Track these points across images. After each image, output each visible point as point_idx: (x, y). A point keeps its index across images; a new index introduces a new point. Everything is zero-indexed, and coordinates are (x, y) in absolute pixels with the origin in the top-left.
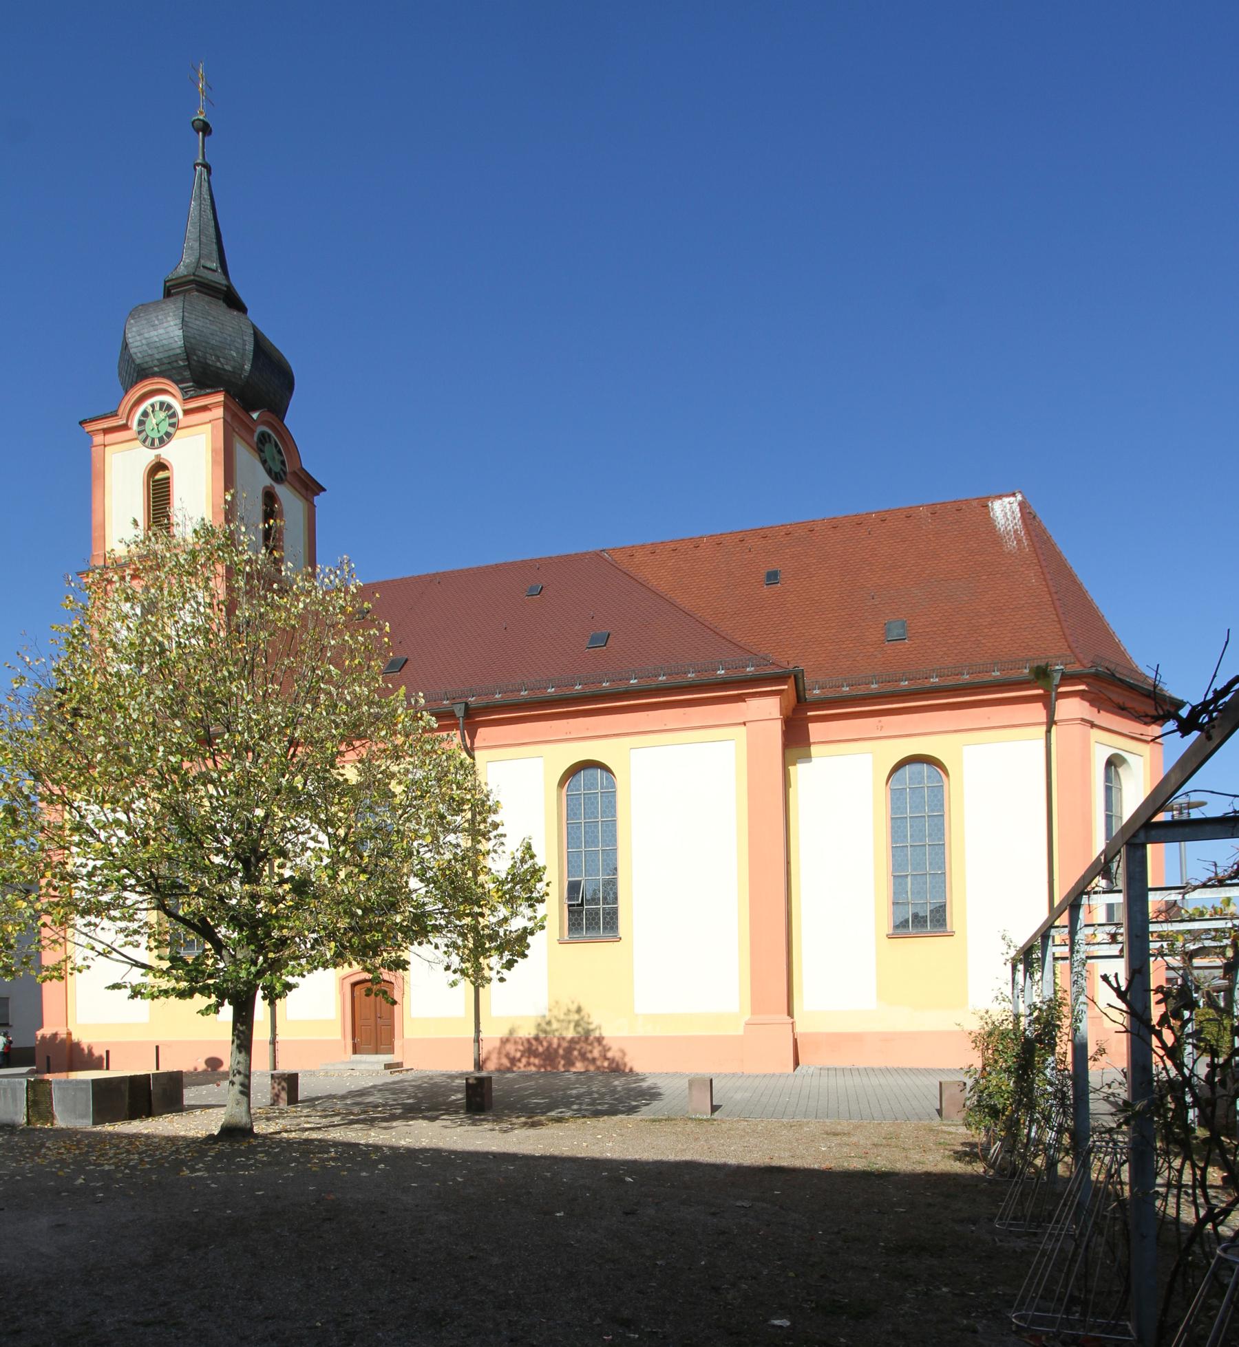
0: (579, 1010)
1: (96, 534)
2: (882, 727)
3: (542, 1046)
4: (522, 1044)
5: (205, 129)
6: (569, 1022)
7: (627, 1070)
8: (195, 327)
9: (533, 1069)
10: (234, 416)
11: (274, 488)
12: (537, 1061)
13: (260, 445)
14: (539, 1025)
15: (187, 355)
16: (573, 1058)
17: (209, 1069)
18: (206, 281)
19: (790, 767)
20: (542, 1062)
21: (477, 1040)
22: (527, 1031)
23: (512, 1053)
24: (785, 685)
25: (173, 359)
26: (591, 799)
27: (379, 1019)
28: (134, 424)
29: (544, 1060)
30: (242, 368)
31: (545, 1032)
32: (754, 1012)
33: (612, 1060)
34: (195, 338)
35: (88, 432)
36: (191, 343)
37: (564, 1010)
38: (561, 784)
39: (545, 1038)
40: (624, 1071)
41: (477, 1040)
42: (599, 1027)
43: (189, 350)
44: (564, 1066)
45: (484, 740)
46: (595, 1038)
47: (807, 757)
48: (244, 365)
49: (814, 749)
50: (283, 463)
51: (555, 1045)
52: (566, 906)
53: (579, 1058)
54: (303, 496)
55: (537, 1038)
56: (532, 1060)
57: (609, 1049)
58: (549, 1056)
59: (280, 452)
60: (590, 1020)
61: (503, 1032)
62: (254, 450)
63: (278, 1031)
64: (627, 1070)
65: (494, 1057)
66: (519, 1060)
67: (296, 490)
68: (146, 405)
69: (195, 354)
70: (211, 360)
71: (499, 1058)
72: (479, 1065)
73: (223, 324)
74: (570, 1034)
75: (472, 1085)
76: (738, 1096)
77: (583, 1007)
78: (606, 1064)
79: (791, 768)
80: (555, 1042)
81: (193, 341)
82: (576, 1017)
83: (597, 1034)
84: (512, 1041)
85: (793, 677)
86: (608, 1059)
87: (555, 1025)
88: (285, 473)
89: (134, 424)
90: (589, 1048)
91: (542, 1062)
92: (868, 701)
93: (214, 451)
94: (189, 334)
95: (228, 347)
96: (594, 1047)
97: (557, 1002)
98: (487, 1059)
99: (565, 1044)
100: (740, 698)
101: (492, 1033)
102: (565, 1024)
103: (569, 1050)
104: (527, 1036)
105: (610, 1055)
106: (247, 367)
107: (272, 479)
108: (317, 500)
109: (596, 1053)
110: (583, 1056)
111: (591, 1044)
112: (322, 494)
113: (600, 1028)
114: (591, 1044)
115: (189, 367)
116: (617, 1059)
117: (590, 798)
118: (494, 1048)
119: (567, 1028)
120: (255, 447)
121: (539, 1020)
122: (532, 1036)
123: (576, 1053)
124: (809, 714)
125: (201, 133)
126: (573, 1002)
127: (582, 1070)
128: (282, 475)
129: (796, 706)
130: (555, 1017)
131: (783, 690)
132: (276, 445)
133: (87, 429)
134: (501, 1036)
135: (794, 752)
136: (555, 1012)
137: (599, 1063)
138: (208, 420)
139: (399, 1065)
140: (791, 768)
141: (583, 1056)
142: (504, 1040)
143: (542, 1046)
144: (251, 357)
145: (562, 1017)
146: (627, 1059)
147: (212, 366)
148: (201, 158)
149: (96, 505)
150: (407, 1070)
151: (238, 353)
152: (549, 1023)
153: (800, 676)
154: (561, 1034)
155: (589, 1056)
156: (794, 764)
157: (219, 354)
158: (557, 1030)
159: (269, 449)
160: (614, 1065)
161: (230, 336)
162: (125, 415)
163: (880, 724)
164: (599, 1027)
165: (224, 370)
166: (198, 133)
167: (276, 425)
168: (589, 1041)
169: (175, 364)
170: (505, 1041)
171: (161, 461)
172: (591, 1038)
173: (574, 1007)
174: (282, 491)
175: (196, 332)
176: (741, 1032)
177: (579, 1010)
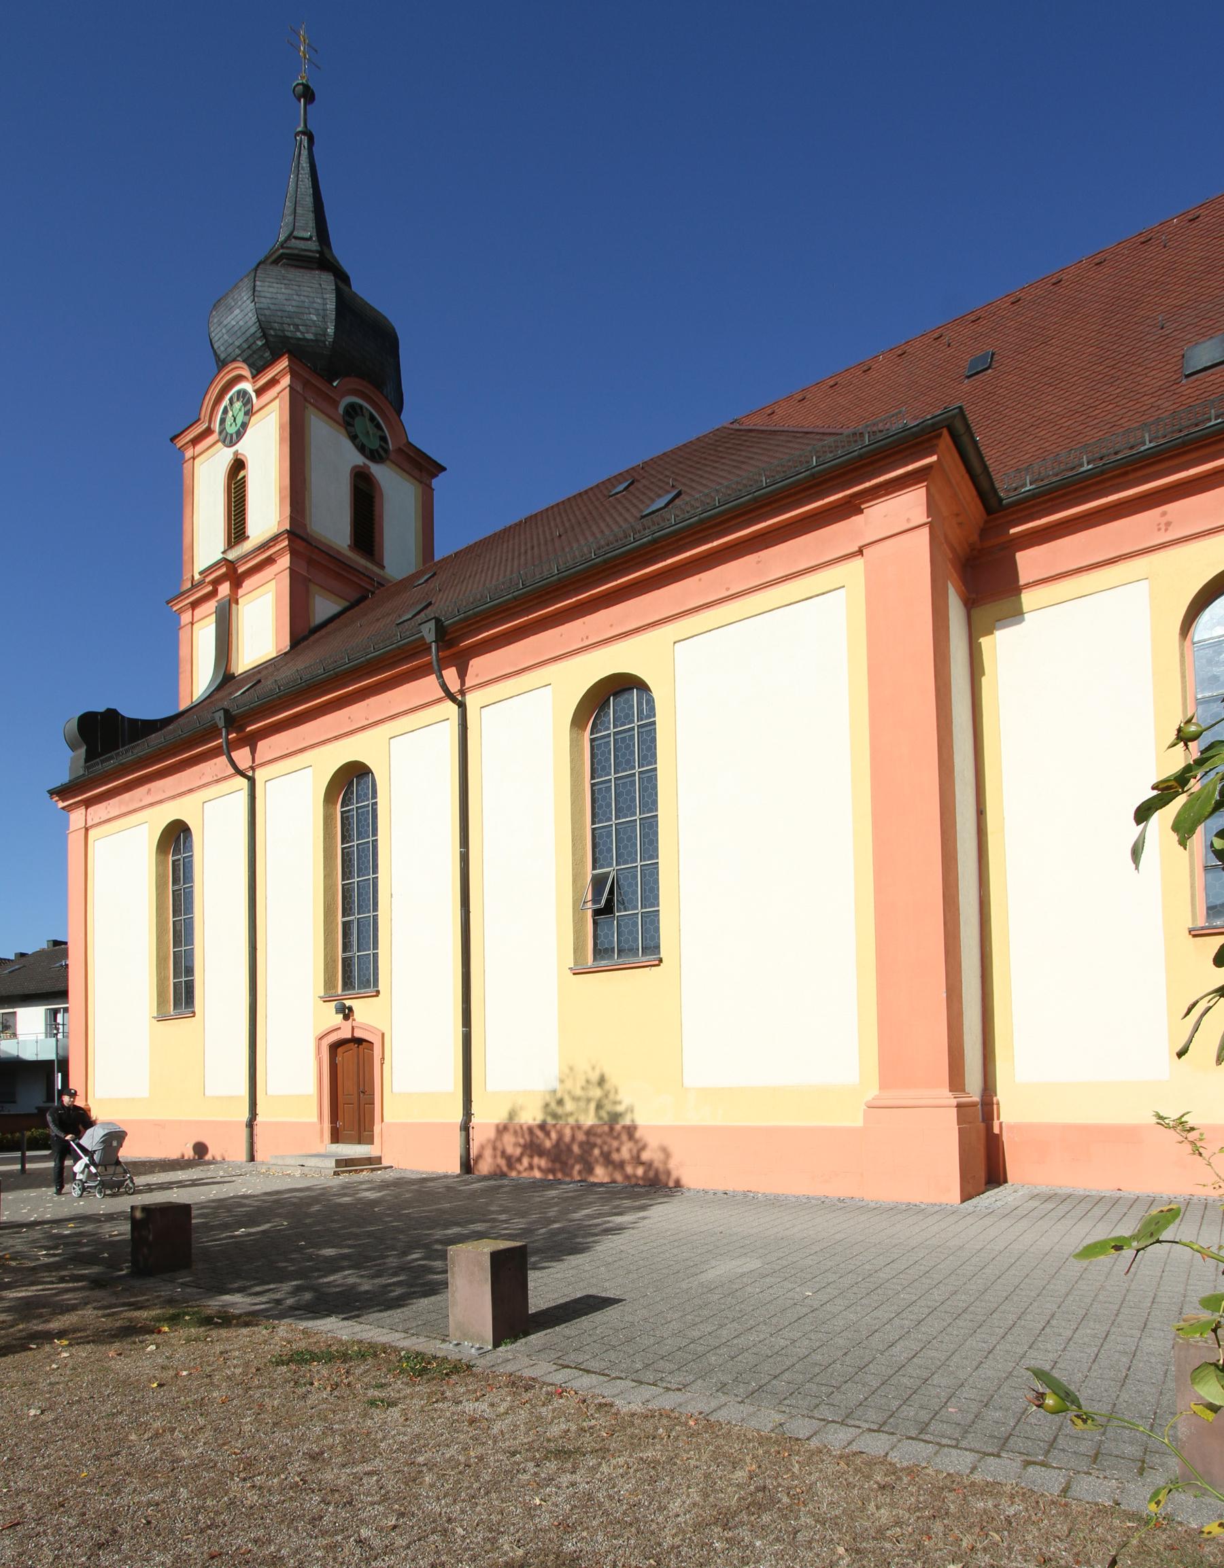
0: (602, 1081)
1: (186, 557)
2: (1168, 524)
3: (550, 1139)
4: (523, 1136)
5: (308, 94)
6: (589, 1100)
7: (671, 1184)
8: (268, 295)
9: (537, 1174)
10: (306, 384)
11: (369, 468)
12: (543, 1163)
13: (347, 418)
14: (547, 1105)
15: (263, 331)
16: (592, 1160)
17: (197, 1157)
18: (296, 252)
19: (982, 640)
20: (550, 1165)
21: (466, 1127)
22: (531, 1116)
23: (510, 1150)
24: (931, 456)
25: (251, 341)
26: (623, 742)
27: (362, 1095)
28: (216, 426)
29: (553, 1161)
30: (325, 334)
31: (555, 1116)
32: (883, 1085)
33: (648, 1165)
34: (269, 308)
35: (179, 449)
36: (265, 315)
37: (581, 1082)
38: (578, 721)
39: (554, 1126)
40: (666, 1186)
41: (466, 1127)
42: (631, 1109)
43: (264, 327)
44: (580, 1172)
45: (477, 675)
46: (624, 1127)
47: (1017, 614)
48: (326, 329)
49: (1028, 599)
50: (383, 439)
51: (567, 1138)
52: (589, 913)
53: (601, 1160)
54: (415, 478)
55: (543, 1127)
56: (536, 1160)
57: (644, 1148)
58: (560, 1156)
59: (378, 427)
60: (619, 1098)
61: (500, 1117)
62: (340, 425)
63: (475, 1108)
64: (671, 1184)
65: (488, 1153)
66: (519, 1160)
67: (407, 472)
68: (226, 402)
69: (271, 329)
70: (290, 331)
71: (495, 1157)
72: (467, 1166)
73: (299, 286)
74: (589, 1120)
75: (141, 1220)
76: (719, 1270)
77: (607, 1077)
78: (640, 1171)
79: (985, 641)
80: (568, 1133)
81: (267, 312)
82: (597, 1093)
83: (627, 1121)
84: (512, 1130)
85: (945, 431)
86: (642, 1163)
87: (569, 1106)
88: (386, 451)
89: (216, 426)
90: (615, 1144)
91: (550, 1165)
92: (1131, 476)
93: (281, 427)
94: (262, 306)
95: (307, 311)
96: (622, 1143)
97: (571, 1069)
98: (479, 1157)
99: (581, 1137)
100: (851, 508)
101: (487, 1116)
102: (582, 1104)
103: (587, 1146)
104: (531, 1122)
105: (645, 1156)
106: (331, 331)
107: (367, 458)
108: (435, 483)
109: (625, 1153)
110: (607, 1159)
111: (618, 1137)
112: (442, 475)
113: (632, 1111)
114: (618, 1137)
115: (267, 345)
116: (656, 1164)
117: (623, 739)
118: (489, 1141)
119: (586, 1111)
120: (341, 421)
121: (548, 1098)
122: (538, 1122)
123: (596, 1152)
124: (1012, 531)
125: (302, 100)
126: (593, 1068)
127: (606, 1180)
128: (382, 453)
129: (986, 522)
130: (569, 1093)
131: (929, 467)
132: (372, 419)
133: (179, 445)
134: (497, 1121)
135: (983, 613)
136: (569, 1084)
137: (629, 1170)
138: (276, 395)
139: (378, 1160)
140: (985, 641)
141: (607, 1159)
142: (501, 1127)
143: (550, 1139)
144: (333, 317)
145: (578, 1092)
146: (672, 1165)
147: (291, 338)
148: (302, 125)
149: (187, 526)
150: (386, 1168)
151: (317, 315)
152: (560, 1102)
153: (959, 425)
154: (577, 1121)
155: (615, 1156)
156: (989, 631)
157: (297, 321)
158: (571, 1114)
159: (360, 424)
160: (651, 1174)
161: (308, 296)
162: (207, 418)
163: (1164, 520)
164: (631, 1109)
165: (307, 340)
166: (300, 101)
167: (371, 395)
168: (615, 1134)
169: (254, 347)
170: (502, 1130)
171: (239, 457)
172: (618, 1127)
173: (594, 1077)
174: (383, 474)
175: (268, 301)
176: (856, 1120)
177: (602, 1081)
